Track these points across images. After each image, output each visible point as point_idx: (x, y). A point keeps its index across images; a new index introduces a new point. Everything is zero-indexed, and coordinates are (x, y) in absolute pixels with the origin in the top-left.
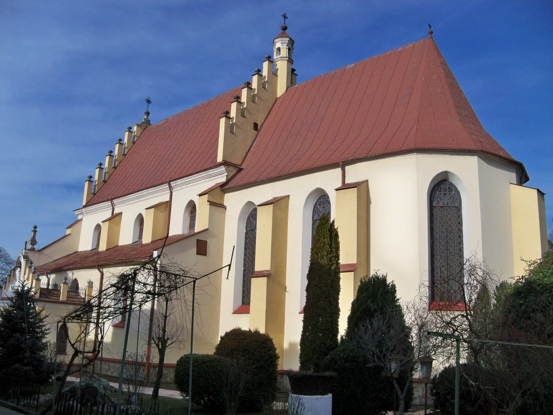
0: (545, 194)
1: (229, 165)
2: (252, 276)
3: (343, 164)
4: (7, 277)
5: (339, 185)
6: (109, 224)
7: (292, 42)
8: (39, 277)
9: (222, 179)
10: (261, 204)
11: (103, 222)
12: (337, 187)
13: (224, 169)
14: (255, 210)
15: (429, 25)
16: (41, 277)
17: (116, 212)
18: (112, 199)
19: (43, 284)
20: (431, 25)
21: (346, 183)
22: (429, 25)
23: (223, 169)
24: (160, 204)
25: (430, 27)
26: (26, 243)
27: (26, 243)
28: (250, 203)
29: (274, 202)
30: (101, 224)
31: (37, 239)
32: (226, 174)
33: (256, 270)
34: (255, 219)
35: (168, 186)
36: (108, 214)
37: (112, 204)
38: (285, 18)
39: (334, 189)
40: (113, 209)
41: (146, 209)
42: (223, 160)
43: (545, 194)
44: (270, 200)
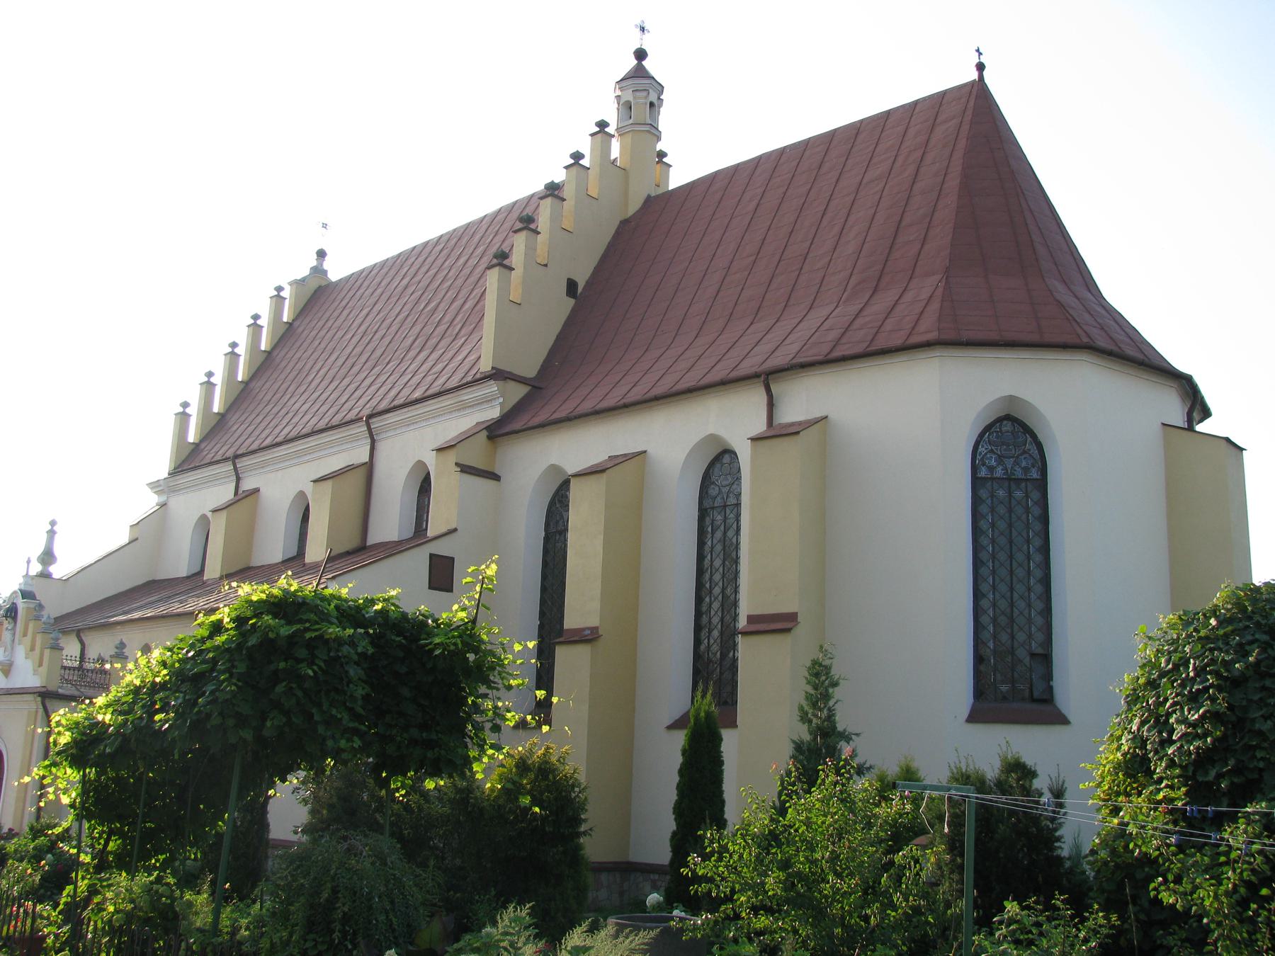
0: (1245, 450)
1: (508, 380)
2: (557, 640)
3: (767, 378)
4: (990, 942)
5: (760, 426)
6: (333, 487)
7: (660, 89)
8: (124, 651)
9: (494, 413)
10: (592, 466)
11: (214, 511)
12: (753, 433)
13: (496, 388)
14: (565, 485)
15: (978, 50)
16: (63, 642)
17: (247, 485)
18: (236, 457)
19: (91, 661)
20: (981, 51)
21: (776, 422)
22: (978, 50)
23: (492, 387)
24: (347, 469)
25: (980, 54)
26: (29, 562)
27: (29, 562)
28: (555, 469)
29: (608, 468)
30: (209, 515)
31: (57, 551)
32: (501, 400)
33: (566, 627)
34: (566, 507)
35: (366, 429)
36: (225, 492)
37: (235, 469)
38: (643, 31)
39: (748, 439)
40: (238, 480)
41: (314, 481)
42: (493, 368)
43: (1245, 450)
44: (601, 463)
